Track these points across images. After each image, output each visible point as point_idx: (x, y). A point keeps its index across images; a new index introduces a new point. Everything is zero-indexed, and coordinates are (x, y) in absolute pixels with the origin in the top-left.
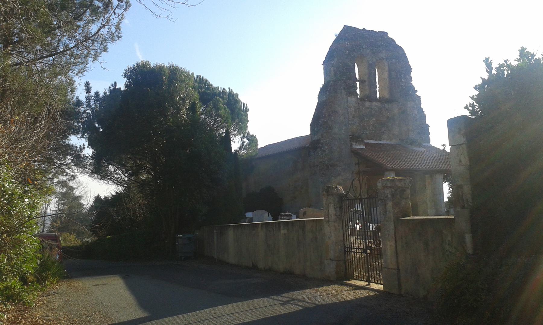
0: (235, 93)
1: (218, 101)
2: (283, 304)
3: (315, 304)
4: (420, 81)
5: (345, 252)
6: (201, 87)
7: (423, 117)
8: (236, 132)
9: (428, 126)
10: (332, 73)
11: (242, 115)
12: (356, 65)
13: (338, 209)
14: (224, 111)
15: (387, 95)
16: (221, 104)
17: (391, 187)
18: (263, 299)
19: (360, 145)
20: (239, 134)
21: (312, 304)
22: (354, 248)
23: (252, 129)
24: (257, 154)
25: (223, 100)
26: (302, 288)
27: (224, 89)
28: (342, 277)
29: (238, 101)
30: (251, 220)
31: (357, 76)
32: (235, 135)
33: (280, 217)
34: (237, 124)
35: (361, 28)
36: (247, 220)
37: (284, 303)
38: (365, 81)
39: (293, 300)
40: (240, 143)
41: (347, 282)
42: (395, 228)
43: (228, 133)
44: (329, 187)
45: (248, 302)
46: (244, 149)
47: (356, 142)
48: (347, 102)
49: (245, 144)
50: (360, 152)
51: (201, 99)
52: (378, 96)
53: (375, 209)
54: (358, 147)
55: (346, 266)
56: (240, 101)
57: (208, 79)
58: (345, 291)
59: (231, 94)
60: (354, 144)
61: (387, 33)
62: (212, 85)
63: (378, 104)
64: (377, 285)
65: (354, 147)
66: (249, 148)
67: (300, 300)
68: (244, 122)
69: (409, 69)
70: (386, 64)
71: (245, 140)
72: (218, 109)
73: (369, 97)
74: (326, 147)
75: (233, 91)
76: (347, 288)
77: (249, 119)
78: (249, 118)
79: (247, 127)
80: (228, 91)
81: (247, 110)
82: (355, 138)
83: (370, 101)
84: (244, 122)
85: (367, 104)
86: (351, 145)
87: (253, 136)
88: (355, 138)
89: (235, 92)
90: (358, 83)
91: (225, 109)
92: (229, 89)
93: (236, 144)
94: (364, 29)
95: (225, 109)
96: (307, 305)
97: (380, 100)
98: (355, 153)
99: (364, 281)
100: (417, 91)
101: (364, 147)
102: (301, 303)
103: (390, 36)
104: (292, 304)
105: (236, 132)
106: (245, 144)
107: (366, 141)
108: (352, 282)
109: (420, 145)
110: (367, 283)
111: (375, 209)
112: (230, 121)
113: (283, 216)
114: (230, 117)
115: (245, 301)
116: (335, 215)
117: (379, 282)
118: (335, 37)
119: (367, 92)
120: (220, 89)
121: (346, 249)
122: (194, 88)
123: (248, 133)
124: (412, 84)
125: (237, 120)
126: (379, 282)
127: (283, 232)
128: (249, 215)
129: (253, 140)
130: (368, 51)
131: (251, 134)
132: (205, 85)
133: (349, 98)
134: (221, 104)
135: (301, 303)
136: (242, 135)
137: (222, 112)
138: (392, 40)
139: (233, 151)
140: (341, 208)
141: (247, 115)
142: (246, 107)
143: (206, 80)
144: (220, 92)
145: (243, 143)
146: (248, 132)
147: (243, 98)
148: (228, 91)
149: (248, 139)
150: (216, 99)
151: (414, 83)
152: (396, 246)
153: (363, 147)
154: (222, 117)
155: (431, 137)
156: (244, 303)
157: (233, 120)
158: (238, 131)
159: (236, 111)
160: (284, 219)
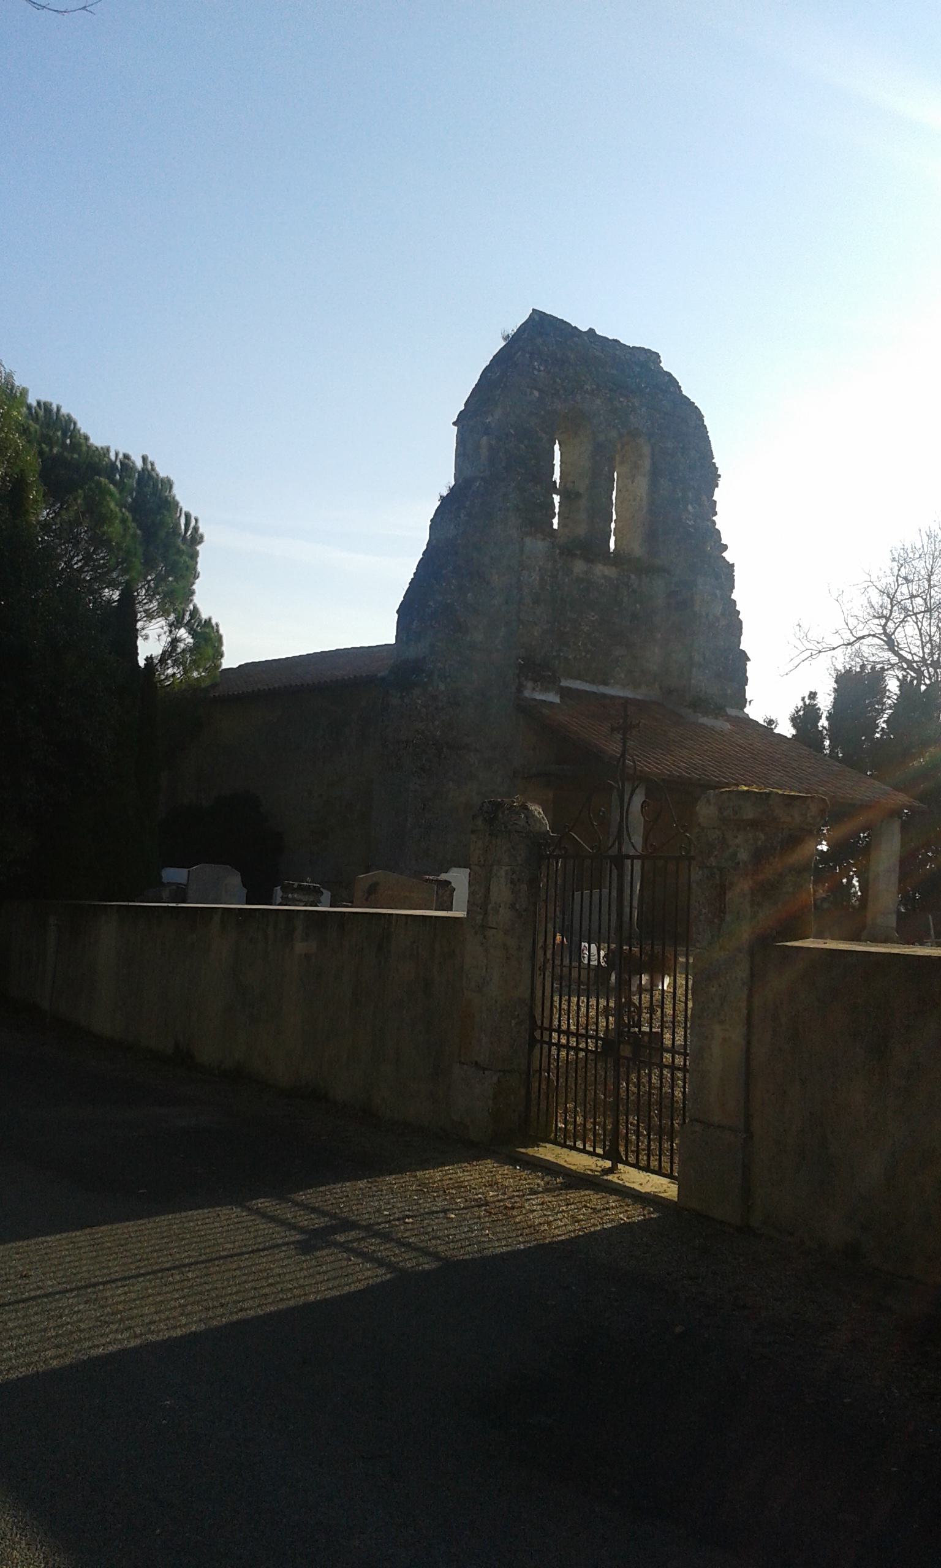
0: (162, 475)
1: (104, 492)
2: (305, 1248)
3: (436, 1256)
4: (745, 517)
5: (532, 1042)
6: (47, 439)
7: (735, 627)
8: (154, 605)
9: (744, 658)
10: (484, 452)
11: (179, 552)
12: (557, 447)
13: (524, 887)
14: (120, 526)
15: (637, 549)
16: (112, 505)
17: (754, 824)
18: (224, 1211)
19: (546, 690)
20: (163, 612)
21: (425, 1252)
22: (559, 1031)
23: (208, 599)
24: (214, 685)
25: (121, 492)
26: (370, 1165)
27: (126, 456)
28: (508, 1135)
29: (171, 505)
30: (180, 893)
31: (557, 476)
32: (150, 616)
33: (278, 891)
34: (160, 579)
35: (584, 329)
36: (165, 894)
37: (311, 1242)
38: (578, 495)
39: (347, 1225)
40: (165, 640)
41: (530, 1151)
42: (752, 975)
43: (128, 600)
44: (499, 805)
45: (163, 1220)
46: (176, 663)
47: (535, 681)
48: (522, 551)
49: (182, 645)
50: (545, 711)
51: (45, 475)
52: (612, 546)
53: (587, 892)
54: (539, 696)
55: (528, 1093)
56: (177, 504)
57: (74, 416)
58: (533, 1192)
59: (150, 476)
60: (530, 685)
61: (658, 355)
62: (86, 438)
63: (611, 572)
64: (643, 1174)
65: (527, 694)
66: (194, 662)
67: (370, 1230)
68: (183, 577)
69: (711, 477)
70: (646, 450)
71: (182, 633)
72: (103, 519)
73: (591, 546)
74: (442, 687)
75: (158, 468)
76: (538, 1181)
77: (199, 568)
78: (201, 566)
79: (193, 593)
80: (139, 464)
81: (196, 539)
82: (536, 669)
83: (589, 561)
84: (183, 577)
85: (579, 566)
86: (520, 688)
87: (208, 622)
88: (536, 669)
89: (162, 472)
90: (557, 499)
91: (124, 521)
92: (145, 459)
93: (152, 641)
94: (591, 330)
95: (124, 521)
96: (409, 1261)
97: (618, 559)
98: (528, 711)
99: (593, 1154)
100: (725, 547)
101: (557, 700)
102: (383, 1250)
103: (666, 366)
104: (344, 1247)
105: (154, 605)
106: (182, 645)
107: (564, 683)
108: (548, 1152)
109: (718, 711)
110: (608, 1164)
111: (587, 892)
112: (139, 567)
113: (293, 890)
114: (140, 550)
115: (149, 1215)
116: (513, 906)
117: (654, 1164)
118: (503, 344)
119: (582, 530)
120: (112, 456)
121: (535, 1031)
122: (25, 431)
123: (195, 612)
124: (714, 523)
125: (161, 567)
126: (654, 1164)
127: (300, 947)
128: (174, 875)
129: (208, 638)
130: (598, 402)
131: (204, 616)
132: (64, 435)
133: (528, 540)
134: (112, 505)
135: (383, 1250)
136: (172, 617)
137: (114, 530)
138: (671, 382)
139: (142, 663)
140: (533, 882)
141: (194, 556)
142: (196, 529)
143: (69, 420)
144: (113, 464)
145: (175, 642)
146: (195, 607)
147: (188, 497)
148: (139, 464)
149: (192, 632)
150: (99, 483)
151: (721, 521)
152: (749, 1043)
153: (553, 698)
154: (110, 550)
155: (750, 692)
156: (147, 1225)
157: (149, 564)
158: (161, 605)
159: (162, 534)
160: (295, 902)
